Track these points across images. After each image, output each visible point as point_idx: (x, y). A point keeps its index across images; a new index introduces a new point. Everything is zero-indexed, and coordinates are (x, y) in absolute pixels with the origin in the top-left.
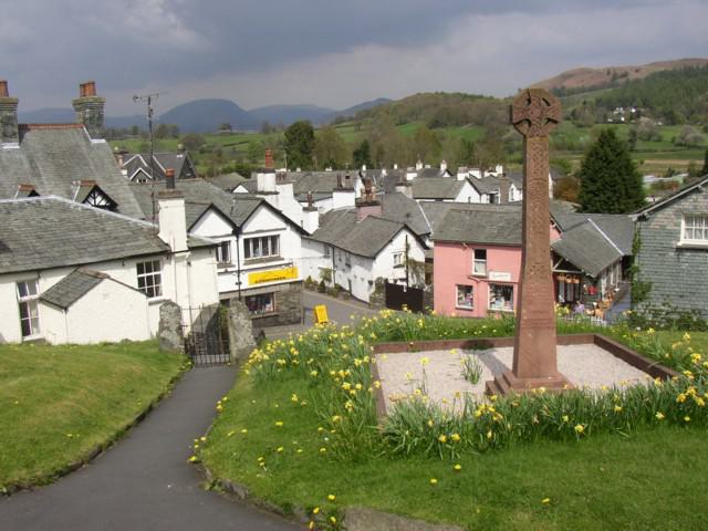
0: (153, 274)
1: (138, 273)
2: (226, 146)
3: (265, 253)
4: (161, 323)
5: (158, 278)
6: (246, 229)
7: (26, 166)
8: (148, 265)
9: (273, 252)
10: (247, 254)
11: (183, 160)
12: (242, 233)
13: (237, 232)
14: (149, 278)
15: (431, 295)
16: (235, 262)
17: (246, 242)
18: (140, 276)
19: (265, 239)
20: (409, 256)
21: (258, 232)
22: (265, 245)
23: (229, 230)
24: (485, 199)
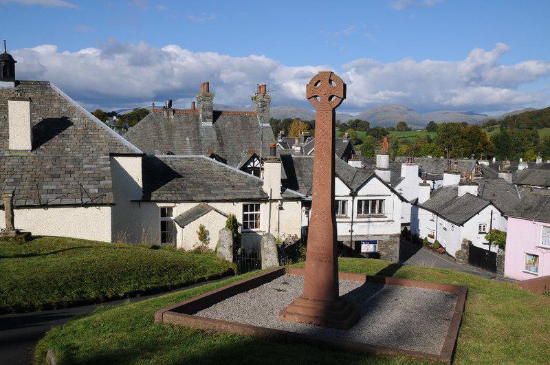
0: (255, 212)
1: (244, 211)
2: (399, 138)
3: (366, 211)
4: (220, 241)
5: (257, 217)
6: (360, 193)
7: (215, 137)
8: (252, 206)
9: (380, 211)
10: (359, 211)
11: (347, 145)
12: (356, 195)
13: (353, 194)
14: (252, 216)
15: (503, 258)
16: (349, 215)
17: (360, 202)
18: (245, 213)
19: (374, 202)
20: (213, 212)
21: (368, 196)
22: (367, 206)
23: (348, 191)
24: (480, 163)
